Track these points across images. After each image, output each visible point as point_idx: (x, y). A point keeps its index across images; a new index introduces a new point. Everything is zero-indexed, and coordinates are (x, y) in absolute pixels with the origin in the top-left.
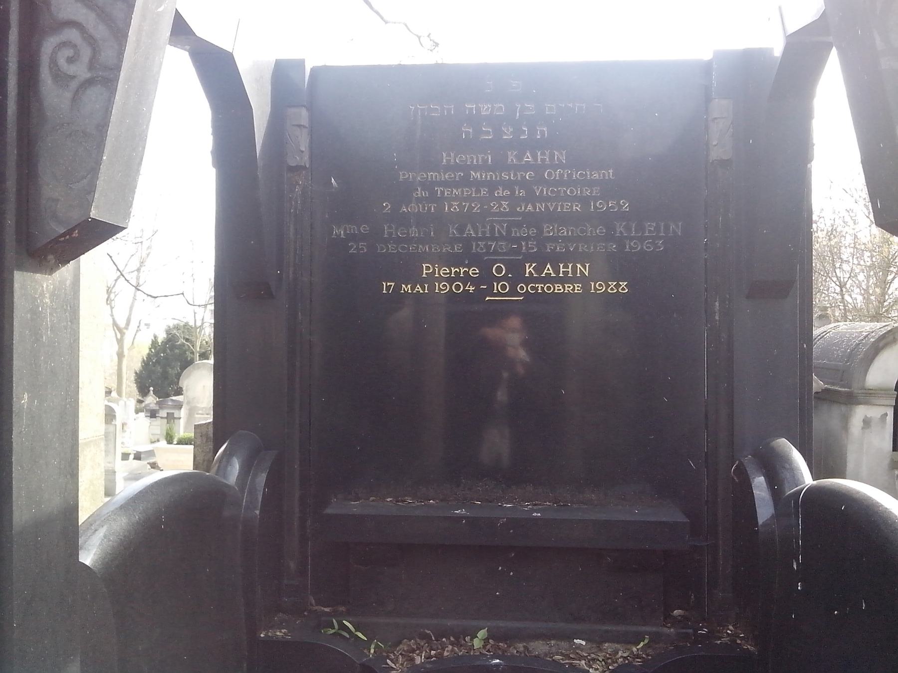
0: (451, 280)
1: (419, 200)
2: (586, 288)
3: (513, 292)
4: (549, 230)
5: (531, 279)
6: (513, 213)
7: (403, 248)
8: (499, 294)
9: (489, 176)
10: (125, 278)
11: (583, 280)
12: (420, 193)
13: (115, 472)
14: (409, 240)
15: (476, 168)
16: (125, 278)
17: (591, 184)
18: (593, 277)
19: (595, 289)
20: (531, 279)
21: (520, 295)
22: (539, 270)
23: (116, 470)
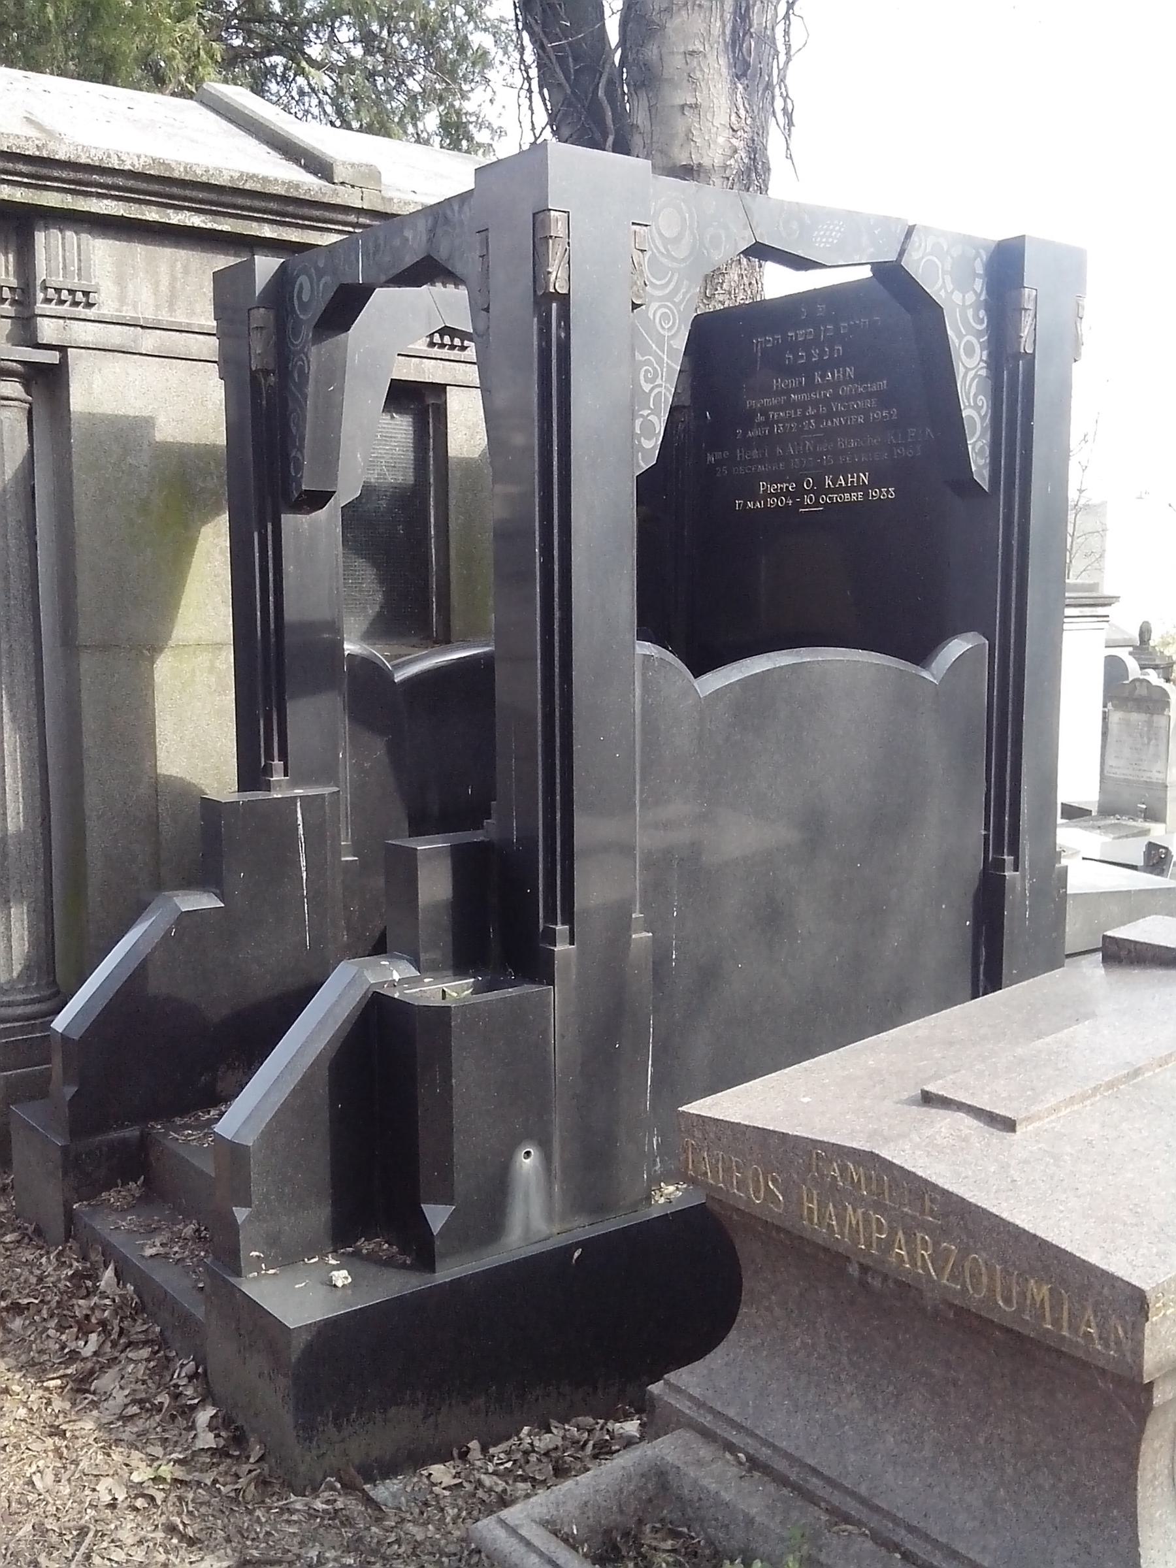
0: (777, 495)
1: (759, 425)
2: (866, 495)
3: (817, 504)
4: (841, 443)
5: (830, 491)
6: (818, 429)
7: (749, 469)
8: (808, 506)
9: (804, 397)
10: (531, 105)
11: (864, 488)
12: (760, 418)
13: (1167, 787)
14: (752, 462)
15: (795, 391)
16: (531, 105)
17: (870, 395)
18: (874, 484)
19: (873, 496)
20: (830, 491)
21: (821, 505)
22: (834, 481)
23: (1169, 781)
